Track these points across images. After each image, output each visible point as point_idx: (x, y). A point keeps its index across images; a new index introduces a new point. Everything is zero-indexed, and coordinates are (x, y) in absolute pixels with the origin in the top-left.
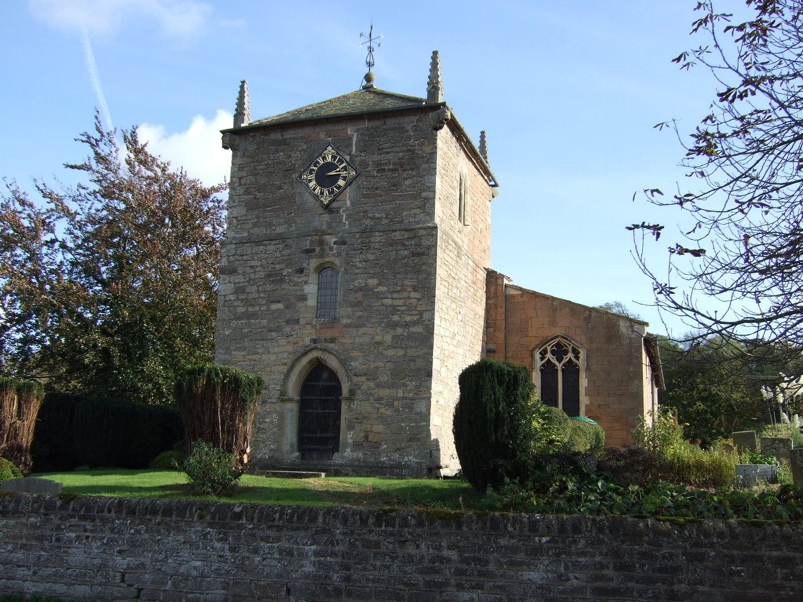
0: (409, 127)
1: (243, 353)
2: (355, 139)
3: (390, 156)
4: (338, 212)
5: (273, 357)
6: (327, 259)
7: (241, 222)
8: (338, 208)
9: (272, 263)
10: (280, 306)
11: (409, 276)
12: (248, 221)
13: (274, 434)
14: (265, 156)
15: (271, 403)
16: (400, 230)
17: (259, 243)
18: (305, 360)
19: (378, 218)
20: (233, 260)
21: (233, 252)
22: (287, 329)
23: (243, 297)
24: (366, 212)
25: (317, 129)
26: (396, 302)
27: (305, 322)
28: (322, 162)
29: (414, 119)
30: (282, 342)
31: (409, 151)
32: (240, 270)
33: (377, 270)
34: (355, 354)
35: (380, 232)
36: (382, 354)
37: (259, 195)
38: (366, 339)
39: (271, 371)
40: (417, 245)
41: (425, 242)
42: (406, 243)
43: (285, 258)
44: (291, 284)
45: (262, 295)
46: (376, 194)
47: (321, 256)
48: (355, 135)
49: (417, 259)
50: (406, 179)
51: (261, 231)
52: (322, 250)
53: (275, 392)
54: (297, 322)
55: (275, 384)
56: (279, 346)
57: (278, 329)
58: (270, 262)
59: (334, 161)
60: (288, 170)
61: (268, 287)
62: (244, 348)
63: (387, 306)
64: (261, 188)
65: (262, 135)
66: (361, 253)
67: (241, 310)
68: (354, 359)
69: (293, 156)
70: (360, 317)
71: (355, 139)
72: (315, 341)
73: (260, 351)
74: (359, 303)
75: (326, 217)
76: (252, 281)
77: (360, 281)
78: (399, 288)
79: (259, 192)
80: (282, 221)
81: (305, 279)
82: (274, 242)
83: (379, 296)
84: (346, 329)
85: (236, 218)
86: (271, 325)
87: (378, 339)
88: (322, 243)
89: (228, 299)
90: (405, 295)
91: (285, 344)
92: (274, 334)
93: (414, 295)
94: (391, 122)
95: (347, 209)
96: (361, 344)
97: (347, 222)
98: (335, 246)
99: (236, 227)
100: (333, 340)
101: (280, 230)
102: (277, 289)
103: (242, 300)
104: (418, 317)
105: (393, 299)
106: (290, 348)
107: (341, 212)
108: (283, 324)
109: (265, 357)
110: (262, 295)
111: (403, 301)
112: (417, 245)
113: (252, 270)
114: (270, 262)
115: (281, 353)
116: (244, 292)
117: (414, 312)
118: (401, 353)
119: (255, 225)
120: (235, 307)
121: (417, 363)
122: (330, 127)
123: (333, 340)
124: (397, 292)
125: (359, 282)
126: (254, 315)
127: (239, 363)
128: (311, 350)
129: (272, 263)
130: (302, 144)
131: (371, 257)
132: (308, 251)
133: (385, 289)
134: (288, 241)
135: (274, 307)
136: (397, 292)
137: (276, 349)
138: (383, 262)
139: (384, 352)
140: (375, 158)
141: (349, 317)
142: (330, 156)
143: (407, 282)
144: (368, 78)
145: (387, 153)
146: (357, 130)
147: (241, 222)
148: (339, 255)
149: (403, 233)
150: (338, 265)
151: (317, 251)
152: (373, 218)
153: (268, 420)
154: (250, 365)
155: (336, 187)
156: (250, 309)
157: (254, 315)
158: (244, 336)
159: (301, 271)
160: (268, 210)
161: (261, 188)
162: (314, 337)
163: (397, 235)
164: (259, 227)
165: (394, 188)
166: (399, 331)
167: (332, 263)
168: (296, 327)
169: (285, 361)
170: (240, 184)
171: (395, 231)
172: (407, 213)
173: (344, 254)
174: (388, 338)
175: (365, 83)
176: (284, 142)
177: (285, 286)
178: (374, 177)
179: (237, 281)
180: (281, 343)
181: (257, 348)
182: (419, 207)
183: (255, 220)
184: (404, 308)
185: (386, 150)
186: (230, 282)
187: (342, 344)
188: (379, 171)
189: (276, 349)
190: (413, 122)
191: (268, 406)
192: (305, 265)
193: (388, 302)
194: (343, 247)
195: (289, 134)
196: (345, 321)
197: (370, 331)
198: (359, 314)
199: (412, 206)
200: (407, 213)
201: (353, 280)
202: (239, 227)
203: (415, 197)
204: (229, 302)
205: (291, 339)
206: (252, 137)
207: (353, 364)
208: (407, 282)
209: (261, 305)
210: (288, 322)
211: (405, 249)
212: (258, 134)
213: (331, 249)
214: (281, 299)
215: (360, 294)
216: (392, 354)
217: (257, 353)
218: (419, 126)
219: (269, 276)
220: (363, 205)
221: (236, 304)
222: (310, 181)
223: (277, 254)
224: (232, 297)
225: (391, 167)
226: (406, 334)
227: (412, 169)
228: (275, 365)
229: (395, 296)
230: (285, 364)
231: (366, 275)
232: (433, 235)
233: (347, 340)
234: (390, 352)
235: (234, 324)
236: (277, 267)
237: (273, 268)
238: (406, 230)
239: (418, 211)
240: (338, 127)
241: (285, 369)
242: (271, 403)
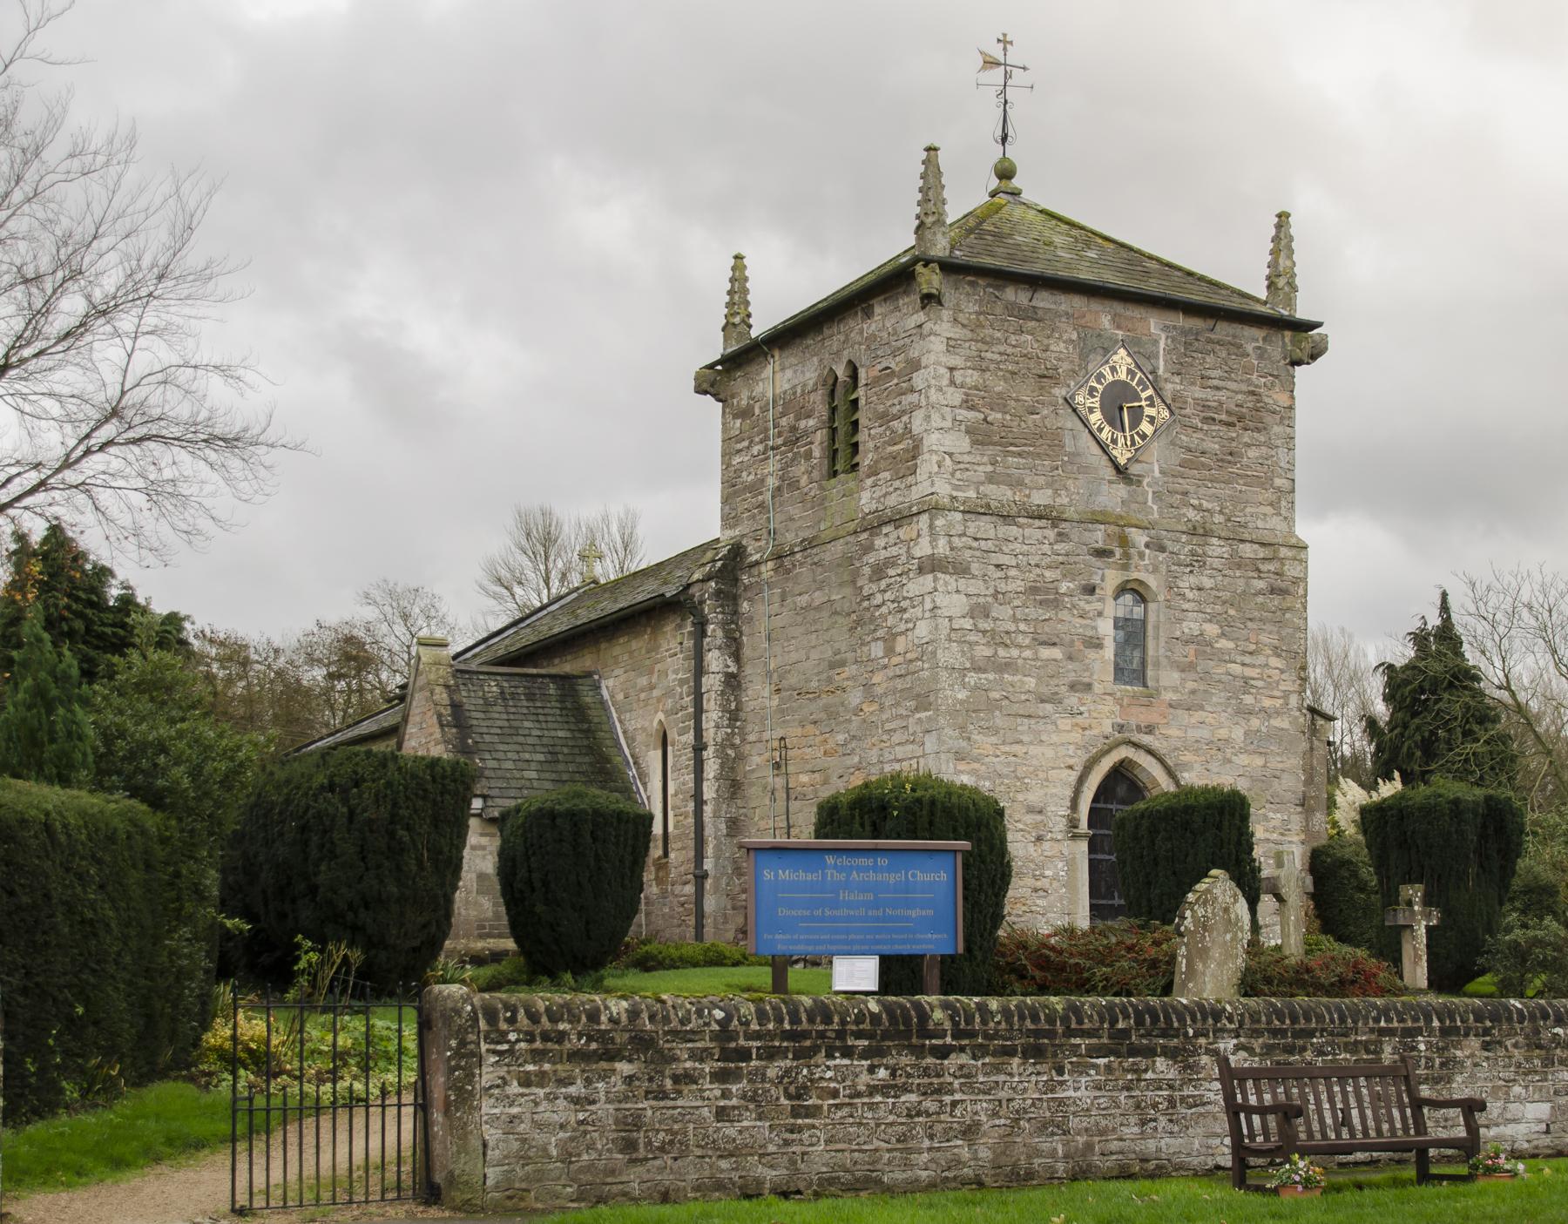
0: (1249, 348)
1: (994, 739)
2: (1162, 345)
3: (1222, 396)
4: (1139, 483)
5: (1050, 753)
6: (1135, 575)
7: (962, 466)
8: (1139, 476)
9: (1037, 566)
10: (1056, 653)
11: (1268, 627)
12: (976, 467)
13: (1061, 899)
14: (998, 335)
15: (1052, 839)
16: (1251, 542)
17: (1007, 518)
18: (1106, 764)
19: (1208, 511)
20: (960, 545)
21: (959, 529)
22: (1072, 700)
23: (986, 625)
24: (1186, 494)
25: (1095, 305)
26: (1249, 672)
27: (1102, 691)
28: (1110, 378)
29: (1259, 333)
30: (1065, 723)
31: (1253, 393)
32: (975, 568)
33: (1218, 608)
34: (1188, 757)
35: (1220, 538)
36: (1230, 761)
37: (995, 416)
38: (1204, 733)
39: (1047, 780)
40: (1277, 574)
41: (1292, 571)
42: (1261, 567)
43: (1061, 559)
44: (1075, 612)
45: (1022, 626)
46: (1203, 465)
47: (1125, 567)
48: (1163, 336)
49: (1276, 600)
50: (1248, 445)
51: (1000, 494)
52: (1127, 555)
53: (1058, 818)
54: (1088, 687)
55: (1056, 805)
56: (1058, 730)
57: (1054, 699)
58: (1033, 563)
59: (1132, 380)
60: (1045, 377)
61: (1033, 612)
62: (996, 731)
63: (1235, 677)
64: (1000, 403)
65: (989, 285)
66: (1191, 572)
67: (983, 651)
68: (1187, 766)
69: (1052, 348)
70: (1193, 692)
71: (1162, 345)
72: (1121, 728)
73: (1025, 738)
74: (1191, 667)
75: (1122, 490)
76: (1000, 596)
77: (1192, 625)
78: (1253, 647)
79: (992, 409)
80: (1041, 480)
81: (1098, 606)
82: (1037, 523)
83: (1223, 658)
84: (1172, 710)
85: (951, 455)
86: (1044, 690)
87: (1223, 733)
88: (1124, 542)
89: (957, 627)
90: (1261, 660)
91: (1068, 728)
92: (1049, 707)
93: (1274, 662)
94: (1224, 330)
95: (1155, 482)
96: (1197, 741)
97: (1155, 507)
98: (1147, 551)
99: (953, 474)
100: (1150, 730)
101: (1040, 498)
102: (1050, 619)
103: (984, 632)
104: (1281, 701)
105: (1244, 665)
106: (1076, 736)
107: (1145, 483)
108: (1064, 689)
109: (1033, 750)
110: (1022, 626)
111: (1258, 671)
112: (1277, 574)
113: (1000, 574)
114: (1033, 563)
115: (1063, 744)
116: (987, 616)
117: (1276, 693)
118: (1259, 761)
119: (991, 479)
120: (970, 644)
121: (1284, 781)
122: (1118, 307)
123: (1150, 730)
124: (1251, 653)
125: (1191, 626)
126: (1007, 666)
127: (987, 760)
128: (1117, 745)
129: (1037, 566)
130: (1070, 330)
131: (1208, 583)
132: (1101, 553)
133: (1231, 645)
134: (1063, 525)
135: (1046, 653)
136: (1251, 653)
137: (1055, 738)
138: (1226, 595)
139: (1234, 758)
140: (1198, 392)
141: (1175, 690)
142: (1124, 369)
143: (1264, 638)
144: (1005, 172)
145: (1217, 388)
146: (1166, 328)
147: (962, 466)
148: (1155, 570)
149: (1256, 547)
150: (1154, 588)
151: (1118, 556)
152: (1199, 508)
153: (1048, 873)
154: (1009, 764)
155: (1137, 433)
156: (1002, 652)
157: (1007, 666)
158: (993, 706)
159: (1091, 590)
160: (1013, 452)
161: (1000, 403)
162: (1119, 720)
163: (1247, 550)
164: (998, 483)
165: (1230, 458)
166: (1255, 723)
167: (1141, 582)
168: (1088, 698)
169: (1071, 762)
170: (952, 383)
171: (1242, 541)
172: (1252, 510)
173: (1163, 568)
174: (1238, 734)
175: (994, 183)
176: (1032, 314)
177: (1064, 615)
178: (1196, 429)
179: (971, 590)
180: (1061, 727)
181: (1022, 733)
182: (1271, 504)
183: (989, 468)
184: (1260, 684)
185: (1215, 382)
186: (958, 591)
187: (1167, 737)
188: (1206, 420)
189: (1055, 738)
190: (1257, 340)
191: (1046, 845)
192: (1096, 580)
193: (1236, 669)
194: (1161, 557)
195: (1045, 300)
196: (1168, 696)
197: (1210, 719)
198: (1190, 685)
199: (1260, 499)
200: (1252, 510)
201: (1180, 621)
202: (958, 475)
203: (1265, 482)
204: (960, 633)
205: (1079, 719)
206: (972, 284)
207: (1186, 775)
208: (1264, 638)
209: (1019, 646)
210: (1073, 687)
211: (1260, 578)
212: (980, 282)
213: (1141, 555)
214: (1057, 640)
215: (1191, 649)
216: (1246, 763)
217: (1019, 742)
218: (1266, 350)
219: (1034, 590)
220: (1181, 481)
221: (972, 637)
222: (1091, 410)
223: (1046, 548)
224: (967, 624)
225: (1224, 417)
226: (1264, 729)
227: (1258, 430)
228: (1053, 768)
229: (1247, 659)
230: (1071, 767)
231: (1200, 615)
232: (1301, 561)
233: (1173, 732)
234: (1243, 759)
235: (972, 678)
236: (1048, 574)
237: (1038, 576)
238: (1263, 544)
239: (1269, 510)
240: (1134, 312)
241: (1073, 776)
242: (1052, 839)
